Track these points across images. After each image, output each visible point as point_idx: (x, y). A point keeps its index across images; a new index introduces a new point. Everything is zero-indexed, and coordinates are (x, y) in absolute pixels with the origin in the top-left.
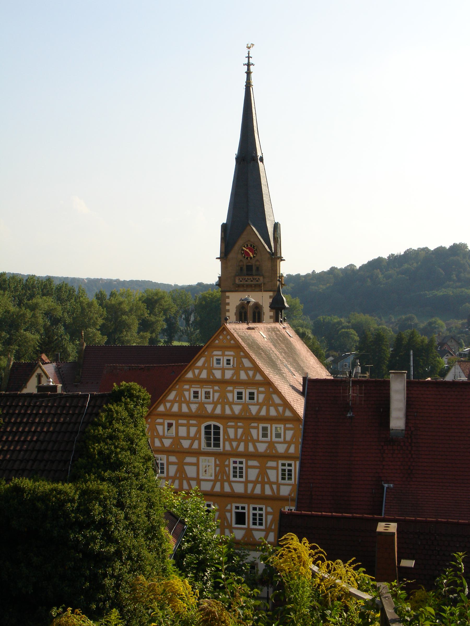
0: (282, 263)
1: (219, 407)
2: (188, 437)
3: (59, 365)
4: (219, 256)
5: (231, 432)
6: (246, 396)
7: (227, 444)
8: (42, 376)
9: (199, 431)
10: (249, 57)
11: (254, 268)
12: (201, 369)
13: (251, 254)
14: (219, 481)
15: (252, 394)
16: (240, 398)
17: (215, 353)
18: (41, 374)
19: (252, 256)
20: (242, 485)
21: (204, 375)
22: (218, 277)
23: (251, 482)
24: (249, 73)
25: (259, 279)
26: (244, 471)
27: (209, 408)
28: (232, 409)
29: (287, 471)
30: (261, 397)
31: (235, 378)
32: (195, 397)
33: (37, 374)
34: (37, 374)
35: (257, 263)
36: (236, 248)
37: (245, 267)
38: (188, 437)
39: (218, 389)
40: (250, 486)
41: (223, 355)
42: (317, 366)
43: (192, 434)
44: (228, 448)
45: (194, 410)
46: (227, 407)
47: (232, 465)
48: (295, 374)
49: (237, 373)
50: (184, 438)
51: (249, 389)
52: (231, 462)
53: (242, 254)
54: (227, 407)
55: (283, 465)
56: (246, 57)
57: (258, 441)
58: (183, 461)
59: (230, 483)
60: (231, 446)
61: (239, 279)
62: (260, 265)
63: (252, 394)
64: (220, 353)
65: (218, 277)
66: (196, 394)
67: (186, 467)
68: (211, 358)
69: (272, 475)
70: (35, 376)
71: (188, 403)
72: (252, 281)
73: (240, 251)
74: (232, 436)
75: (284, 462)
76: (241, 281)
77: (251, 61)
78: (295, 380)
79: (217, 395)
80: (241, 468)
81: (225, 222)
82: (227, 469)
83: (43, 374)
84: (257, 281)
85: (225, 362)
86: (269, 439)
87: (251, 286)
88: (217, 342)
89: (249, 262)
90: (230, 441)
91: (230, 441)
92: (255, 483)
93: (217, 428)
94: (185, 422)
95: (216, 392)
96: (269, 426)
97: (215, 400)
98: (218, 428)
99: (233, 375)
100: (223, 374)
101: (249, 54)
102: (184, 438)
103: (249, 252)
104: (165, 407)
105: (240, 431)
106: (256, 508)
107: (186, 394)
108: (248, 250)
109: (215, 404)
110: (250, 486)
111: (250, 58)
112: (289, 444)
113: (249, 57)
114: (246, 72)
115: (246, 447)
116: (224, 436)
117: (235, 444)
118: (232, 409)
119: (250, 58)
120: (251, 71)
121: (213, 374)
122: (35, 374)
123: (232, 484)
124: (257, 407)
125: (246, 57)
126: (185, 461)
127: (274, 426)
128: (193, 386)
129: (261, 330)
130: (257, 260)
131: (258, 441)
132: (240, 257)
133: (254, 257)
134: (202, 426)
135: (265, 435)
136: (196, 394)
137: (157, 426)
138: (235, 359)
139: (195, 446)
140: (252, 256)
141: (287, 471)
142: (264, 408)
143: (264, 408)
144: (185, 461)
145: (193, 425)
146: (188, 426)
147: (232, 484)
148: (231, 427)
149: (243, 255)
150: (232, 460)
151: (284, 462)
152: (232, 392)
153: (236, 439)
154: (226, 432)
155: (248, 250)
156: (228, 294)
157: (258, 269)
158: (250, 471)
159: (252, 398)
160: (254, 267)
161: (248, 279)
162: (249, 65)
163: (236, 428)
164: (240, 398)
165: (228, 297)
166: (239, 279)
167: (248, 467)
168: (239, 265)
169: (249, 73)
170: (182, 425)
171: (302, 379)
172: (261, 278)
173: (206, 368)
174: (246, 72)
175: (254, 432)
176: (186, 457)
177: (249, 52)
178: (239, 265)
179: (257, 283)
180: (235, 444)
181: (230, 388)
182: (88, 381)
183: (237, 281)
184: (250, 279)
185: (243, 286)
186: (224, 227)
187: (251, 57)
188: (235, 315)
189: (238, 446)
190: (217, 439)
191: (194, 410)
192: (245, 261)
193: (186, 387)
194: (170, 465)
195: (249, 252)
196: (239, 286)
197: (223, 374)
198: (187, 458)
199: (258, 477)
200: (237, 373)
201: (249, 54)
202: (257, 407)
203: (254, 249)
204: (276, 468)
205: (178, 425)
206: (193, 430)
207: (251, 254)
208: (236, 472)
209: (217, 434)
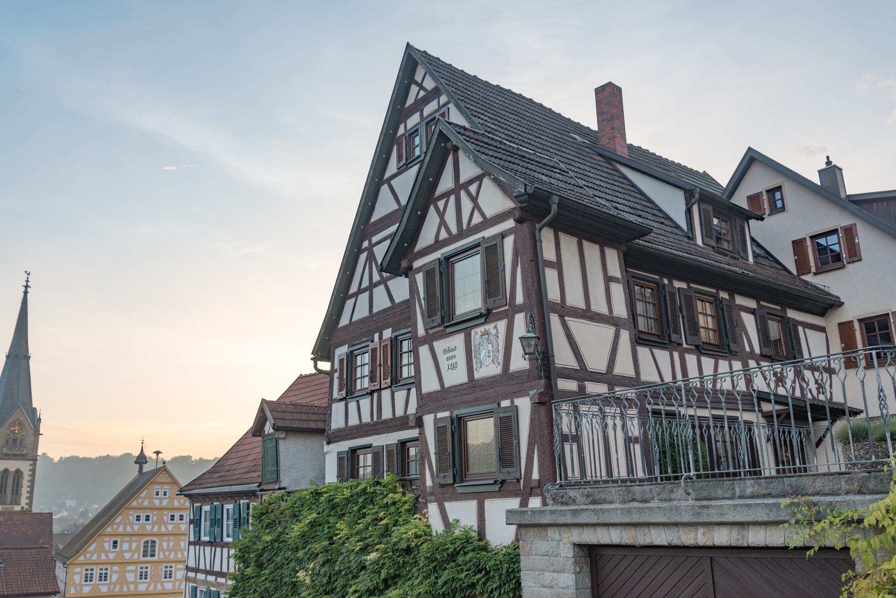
2: (130, 550)
5: (165, 544)
7: (161, 554)
9: (138, 546)
10: (27, 281)
11: (19, 442)
17: (156, 487)
20: (171, 584)
21: (146, 503)
23: (178, 580)
24: (26, 293)
26: (173, 573)
28: (166, 528)
31: (170, 505)
32: (171, 520)
37: (11, 440)
38: (130, 550)
40: (177, 584)
41: (162, 488)
44: (162, 556)
46: (163, 526)
47: (164, 569)
52: (164, 567)
54: (163, 526)
55: (166, 567)
60: (164, 554)
69: (130, 577)
71: (132, 525)
74: (165, 547)
75: (166, 565)
77: (29, 284)
79: (155, 518)
80: (171, 571)
82: (160, 573)
85: (160, 493)
87: (16, 455)
90: (164, 551)
91: (164, 551)
92: (115, 584)
93: (154, 542)
94: (128, 539)
99: (168, 503)
100: (161, 503)
101: (28, 278)
105: (172, 544)
107: (131, 518)
109: (153, 524)
110: (177, 584)
113: (27, 281)
118: (166, 528)
130: (22, 436)
131: (109, 551)
139: (136, 556)
148: (165, 541)
150: (164, 565)
151: (166, 565)
152: (133, 515)
153: (168, 550)
154: (161, 545)
157: (21, 442)
162: (27, 287)
167: (112, 572)
169: (26, 293)
170: (126, 541)
172: (25, 449)
185: (9, 455)
189: (169, 555)
190: (153, 551)
196: (6, 455)
197: (161, 503)
201: (28, 278)
204: (80, 573)
205: (122, 542)
206: (134, 545)
209: (153, 546)
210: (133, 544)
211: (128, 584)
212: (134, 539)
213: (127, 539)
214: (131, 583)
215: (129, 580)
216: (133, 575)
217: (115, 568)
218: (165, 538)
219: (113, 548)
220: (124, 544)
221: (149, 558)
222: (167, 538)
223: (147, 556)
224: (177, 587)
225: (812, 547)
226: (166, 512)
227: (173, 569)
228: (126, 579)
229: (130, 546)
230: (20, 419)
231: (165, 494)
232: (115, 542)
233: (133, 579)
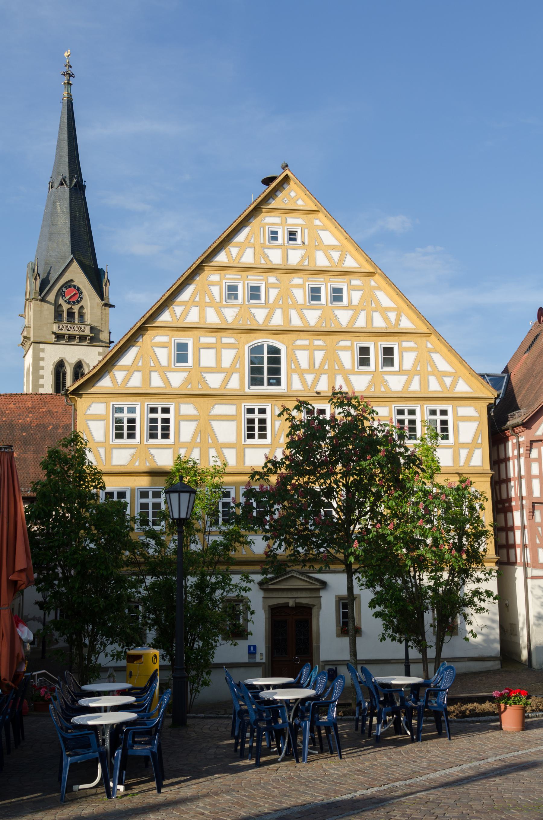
1: (278, 313)
2: (218, 369)
5: (303, 357)
9: (238, 358)
14: (478, 448)
23: (464, 446)
28: (302, 317)
29: (160, 421)
30: (356, 296)
31: (306, 263)
38: (218, 369)
39: (276, 281)
40: (464, 453)
45: (230, 320)
46: (294, 314)
50: (211, 370)
58: (210, 412)
60: (303, 381)
66: (232, 291)
67: (215, 424)
68: (262, 229)
74: (304, 363)
80: (412, 422)
90: (302, 373)
91: (302, 373)
94: (212, 340)
95: (272, 288)
97: (271, 300)
98: (277, 351)
99: (303, 258)
100: (285, 257)
102: (211, 370)
105: (319, 355)
106: (153, 497)
107: (216, 290)
109: (356, 310)
110: (464, 453)
112: (229, 372)
117: (309, 378)
121: (266, 256)
126: (213, 413)
136: (232, 291)
137: (298, 353)
138: (306, 231)
141: (257, 422)
142: (363, 314)
143: (363, 314)
144: (213, 413)
145: (230, 346)
148: (302, 348)
153: (311, 370)
154: (292, 358)
163: (312, 350)
167: (458, 419)
170: (208, 346)
173: (253, 246)
176: (216, 404)
180: (309, 378)
189: (316, 381)
190: (275, 371)
191: (230, 320)
194: (183, 420)
197: (285, 257)
198: (216, 406)
199: (194, 437)
206: (228, 356)
208: (130, 428)
210: (316, 353)
211: (220, 447)
212: (228, 340)
213: (210, 339)
214: (229, 446)
215: (222, 439)
216: (231, 426)
217: (187, 409)
218: (302, 342)
219: (369, 365)
220: (405, 355)
221: (265, 389)
222: (306, 342)
223: (262, 384)
224: (462, 463)
225: (157, 670)
226: (298, 280)
227: (449, 418)
228: (217, 440)
229: (219, 359)
231: (292, 235)
232: (182, 347)
233: (232, 439)
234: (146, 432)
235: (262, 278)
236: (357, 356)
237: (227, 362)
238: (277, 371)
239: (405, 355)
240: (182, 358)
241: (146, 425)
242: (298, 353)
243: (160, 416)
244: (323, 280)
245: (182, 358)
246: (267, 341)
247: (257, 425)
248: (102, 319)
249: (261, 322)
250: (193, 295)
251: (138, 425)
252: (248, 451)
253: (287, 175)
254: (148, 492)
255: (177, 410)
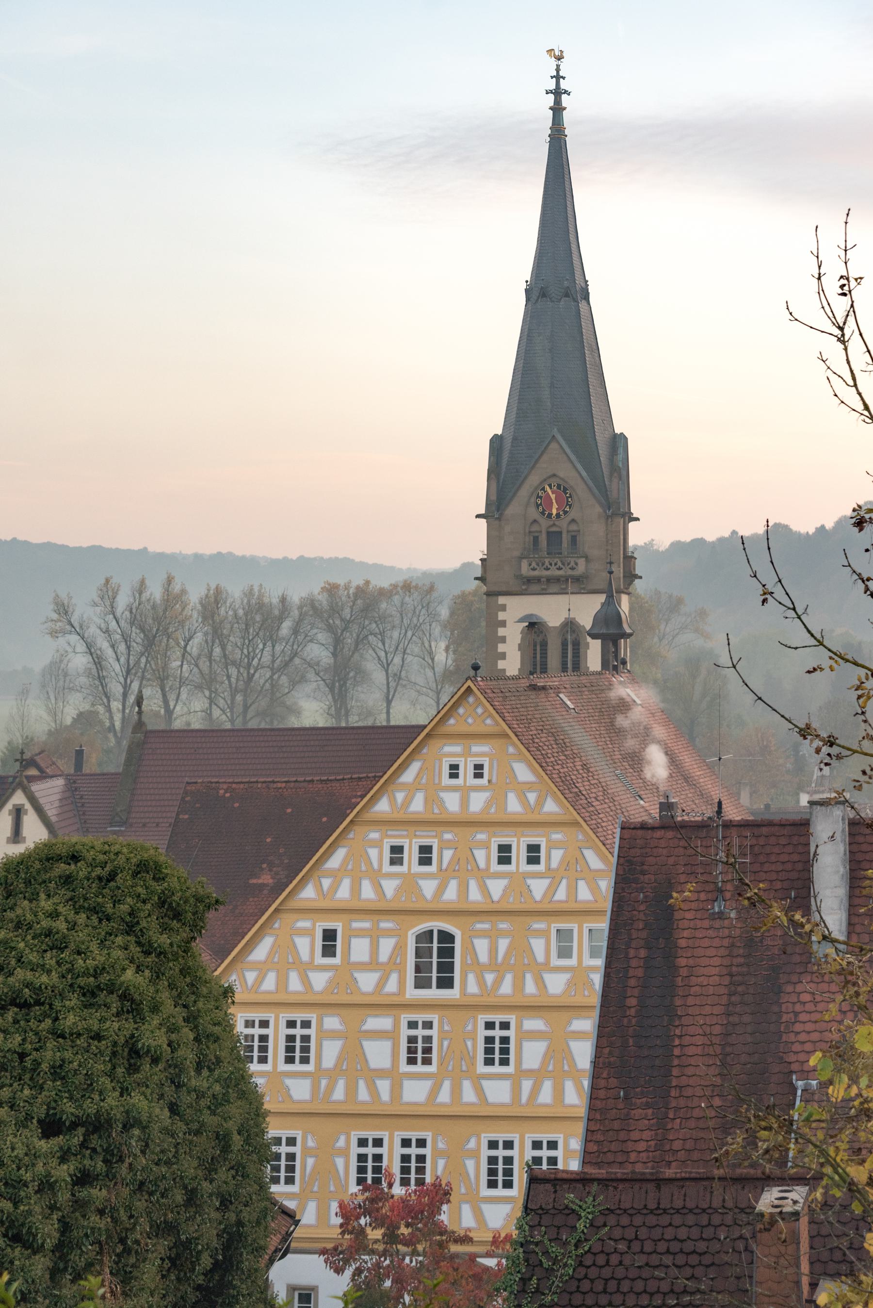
0: (632, 525)
2: (372, 964)
3: (75, 782)
4: (483, 511)
5: (482, 946)
6: (519, 854)
8: (26, 813)
9: (399, 948)
11: (565, 538)
12: (412, 790)
13: (555, 506)
15: (533, 849)
16: (504, 860)
17: (448, 749)
18: (23, 805)
19: (554, 512)
20: (506, 1085)
21: (418, 805)
22: (481, 560)
25: (576, 564)
27: (428, 888)
33: (14, 805)
34: (14, 805)
35: (574, 527)
36: (524, 492)
38: (372, 964)
40: (527, 1085)
41: (467, 753)
42: (698, 773)
43: (384, 957)
44: (473, 987)
45: (496, 897)
48: (643, 797)
49: (498, 799)
51: (527, 836)
53: (538, 506)
56: (552, 77)
57: (546, 966)
59: (477, 1080)
60: (481, 982)
61: (530, 565)
62: (579, 531)
63: (533, 849)
64: (458, 749)
65: (481, 560)
66: (505, 855)
70: (7, 813)
71: (376, 877)
72: (560, 569)
73: (533, 500)
74: (483, 957)
76: (534, 569)
77: (564, 85)
78: (642, 810)
81: (500, 432)
83: (28, 806)
84: (572, 569)
85: (471, 771)
86: (573, 962)
87: (558, 580)
88: (452, 721)
89: (554, 525)
91: (480, 970)
92: (538, 1076)
94: (366, 925)
96: (575, 927)
99: (488, 804)
100: (465, 802)
102: (363, 967)
103: (554, 501)
104: (319, 887)
105: (503, 944)
107: (373, 853)
108: (553, 496)
110: (527, 1085)
111: (561, 80)
113: (558, 77)
114: (551, 108)
115: (519, 984)
116: (463, 962)
117: (490, 978)
119: (561, 80)
120: (564, 105)
122: (9, 806)
123: (485, 1083)
124: (546, 882)
125: (552, 77)
127: (586, 926)
128: (389, 833)
129: (564, 690)
131: (546, 966)
132: (533, 513)
133: (558, 515)
134: (410, 933)
135: (564, 953)
137: (477, 942)
140: (554, 512)
145: (388, 933)
146: (375, 937)
147: (485, 1083)
148: (483, 934)
149: (541, 508)
150: (483, 1018)
153: (493, 965)
155: (553, 496)
156: (502, 600)
157: (574, 540)
158: (527, 1046)
159: (533, 860)
160: (564, 535)
161: (551, 564)
162: (558, 93)
163: (493, 937)
164: (504, 860)
165: (503, 608)
166: (530, 565)
168: (530, 532)
171: (658, 806)
174: (551, 108)
175: (538, 946)
177: (558, 66)
178: (530, 532)
179: (570, 572)
180: (490, 978)
181: (481, 837)
182: (148, 820)
183: (525, 570)
184: (556, 564)
185: (538, 580)
186: (496, 443)
187: (564, 78)
188: (519, 650)
189: (498, 982)
190: (446, 967)
192: (544, 523)
193: (374, 835)
195: (554, 501)
196: (529, 581)
197: (465, 802)
200: (498, 799)
202: (546, 882)
203: (566, 494)
206: (386, 946)
207: (555, 506)
209: (447, 953)
211: (373, 1075)
212: (386, 924)
214: (381, 1073)
216: (386, 1046)
217: (332, 1023)
222: (486, 926)
230: (561, 474)
232: (330, 936)
234: (282, 1054)
235: (405, 833)
236: (319, 942)
237: (384, 955)
238: (450, 967)
239: (355, 942)
240: (329, 950)
241: (282, 1044)
242: (477, 942)
243: (298, 1032)
244: (434, 834)
245: (329, 950)
246: (437, 925)
247: (497, 1046)
248: (607, 542)
249: (538, 897)
250: (345, 861)
251: (271, 1044)
252: (407, 1084)
253: (469, 687)
254: (541, 1142)
255: (519, 1025)
